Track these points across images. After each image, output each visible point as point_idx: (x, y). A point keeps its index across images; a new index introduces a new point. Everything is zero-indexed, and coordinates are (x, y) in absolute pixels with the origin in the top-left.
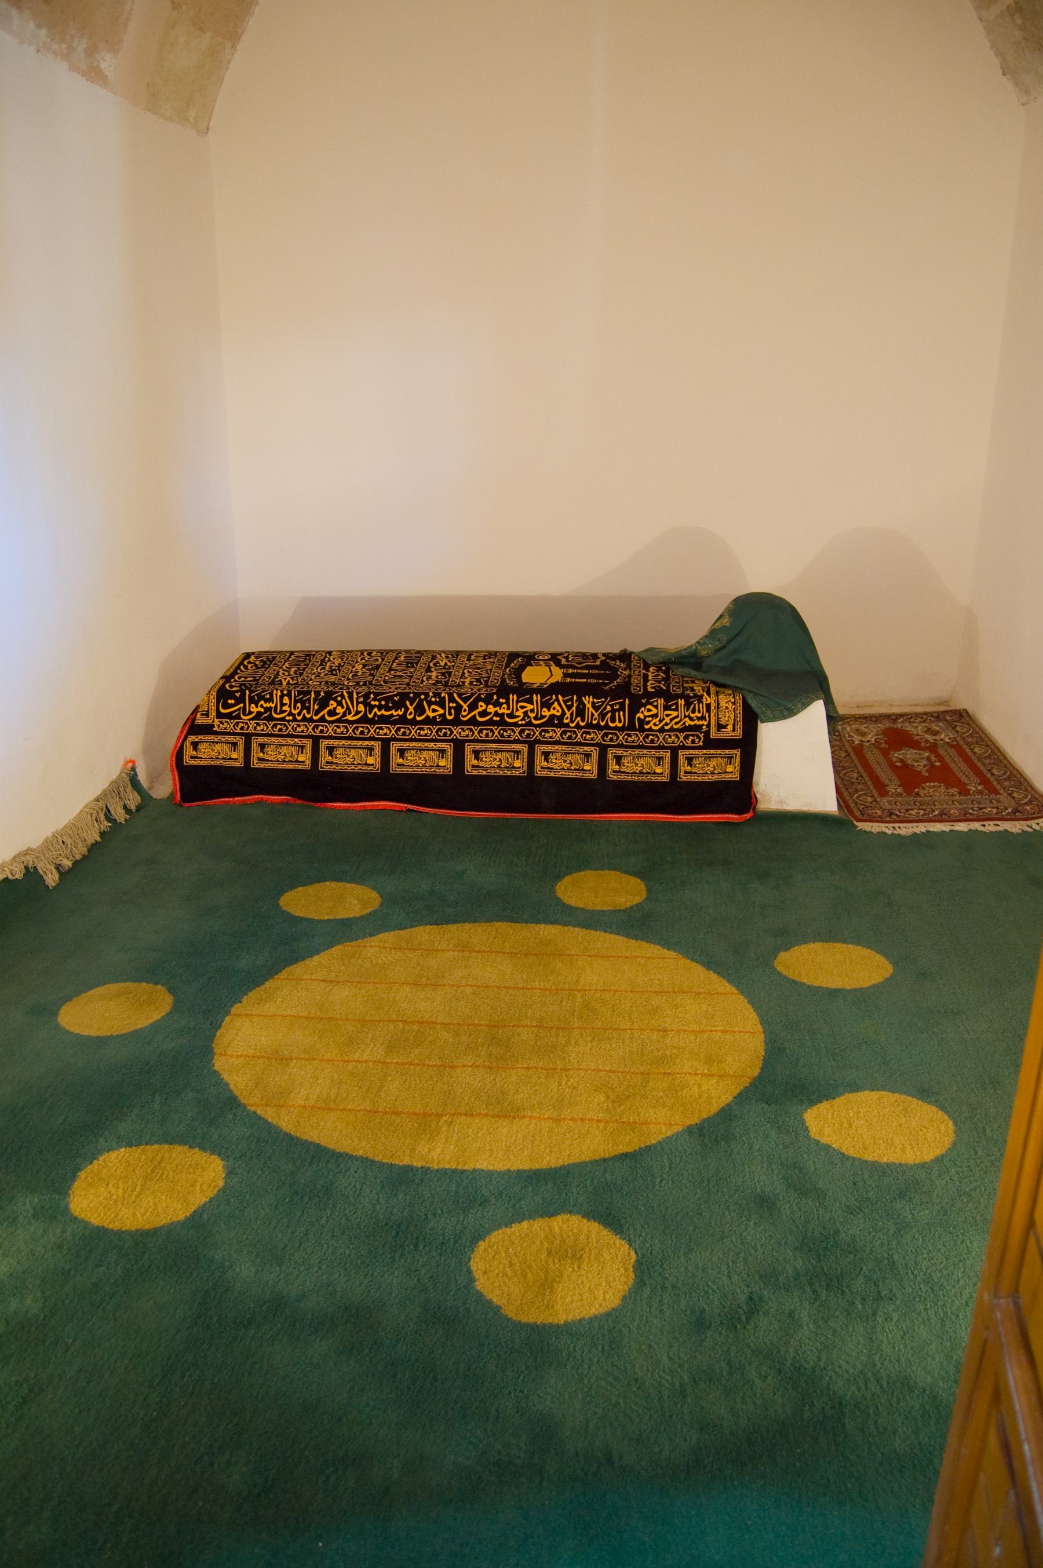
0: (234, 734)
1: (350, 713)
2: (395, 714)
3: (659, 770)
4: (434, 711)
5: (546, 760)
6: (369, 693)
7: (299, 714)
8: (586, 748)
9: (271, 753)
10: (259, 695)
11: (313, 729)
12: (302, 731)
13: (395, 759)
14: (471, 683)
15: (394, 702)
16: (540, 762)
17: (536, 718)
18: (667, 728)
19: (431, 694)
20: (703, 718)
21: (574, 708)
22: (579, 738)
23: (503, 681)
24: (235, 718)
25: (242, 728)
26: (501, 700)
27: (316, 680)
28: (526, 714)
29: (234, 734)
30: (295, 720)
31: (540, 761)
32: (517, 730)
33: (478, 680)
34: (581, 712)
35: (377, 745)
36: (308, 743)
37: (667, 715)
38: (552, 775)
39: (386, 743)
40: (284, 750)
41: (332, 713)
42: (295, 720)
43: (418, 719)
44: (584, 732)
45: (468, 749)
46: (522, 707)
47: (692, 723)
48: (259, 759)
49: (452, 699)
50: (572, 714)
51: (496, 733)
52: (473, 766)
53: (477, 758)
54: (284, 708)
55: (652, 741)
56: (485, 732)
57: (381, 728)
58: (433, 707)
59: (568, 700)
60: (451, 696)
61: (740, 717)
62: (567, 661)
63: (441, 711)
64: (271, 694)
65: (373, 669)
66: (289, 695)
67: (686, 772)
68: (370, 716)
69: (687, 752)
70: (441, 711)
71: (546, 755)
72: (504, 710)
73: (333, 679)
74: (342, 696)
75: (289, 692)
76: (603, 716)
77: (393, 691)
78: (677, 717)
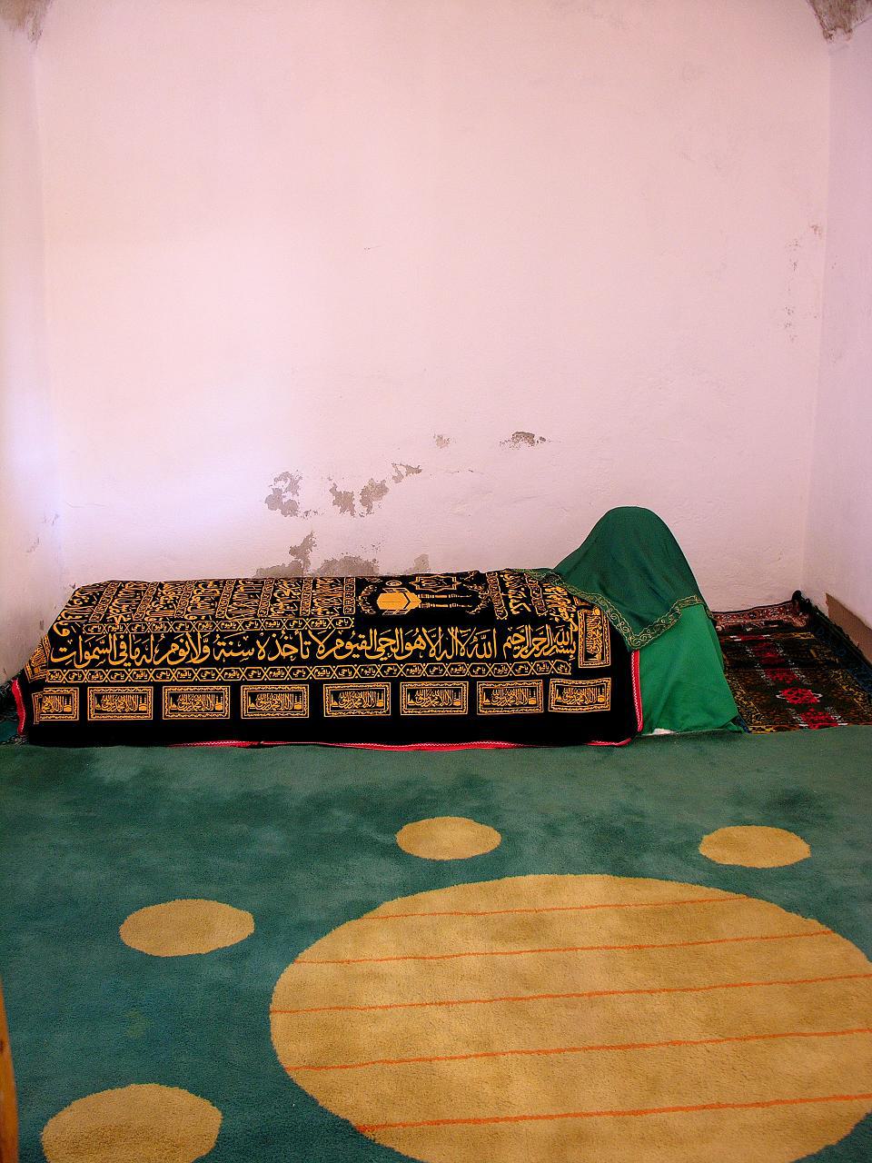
0: (67, 685)
1: (194, 656)
2: (245, 655)
4: (287, 650)
5: (413, 698)
7: (138, 660)
8: (454, 683)
10: (93, 641)
11: (154, 675)
12: (143, 679)
14: (324, 613)
17: (399, 654)
19: (283, 632)
20: (569, 647)
22: (447, 673)
23: (358, 609)
24: (67, 668)
25: (76, 678)
26: (360, 636)
27: (152, 618)
28: (388, 649)
30: (134, 666)
32: (379, 668)
33: (331, 609)
34: (447, 644)
35: (226, 689)
36: (150, 690)
37: (536, 642)
38: (419, 713)
39: (235, 688)
41: (175, 657)
42: (134, 666)
44: (407, 667)
45: (327, 690)
46: (384, 643)
47: (561, 652)
49: (306, 637)
50: (437, 648)
51: (356, 671)
52: (333, 709)
53: (336, 699)
57: (230, 671)
58: (286, 646)
59: (432, 633)
60: (305, 633)
61: (608, 646)
62: (421, 587)
63: (296, 650)
65: (213, 602)
66: (126, 639)
67: (557, 703)
68: (217, 658)
69: (557, 680)
70: (296, 650)
72: (364, 647)
73: (170, 614)
74: (185, 638)
76: (470, 647)
77: (241, 630)
78: (546, 643)
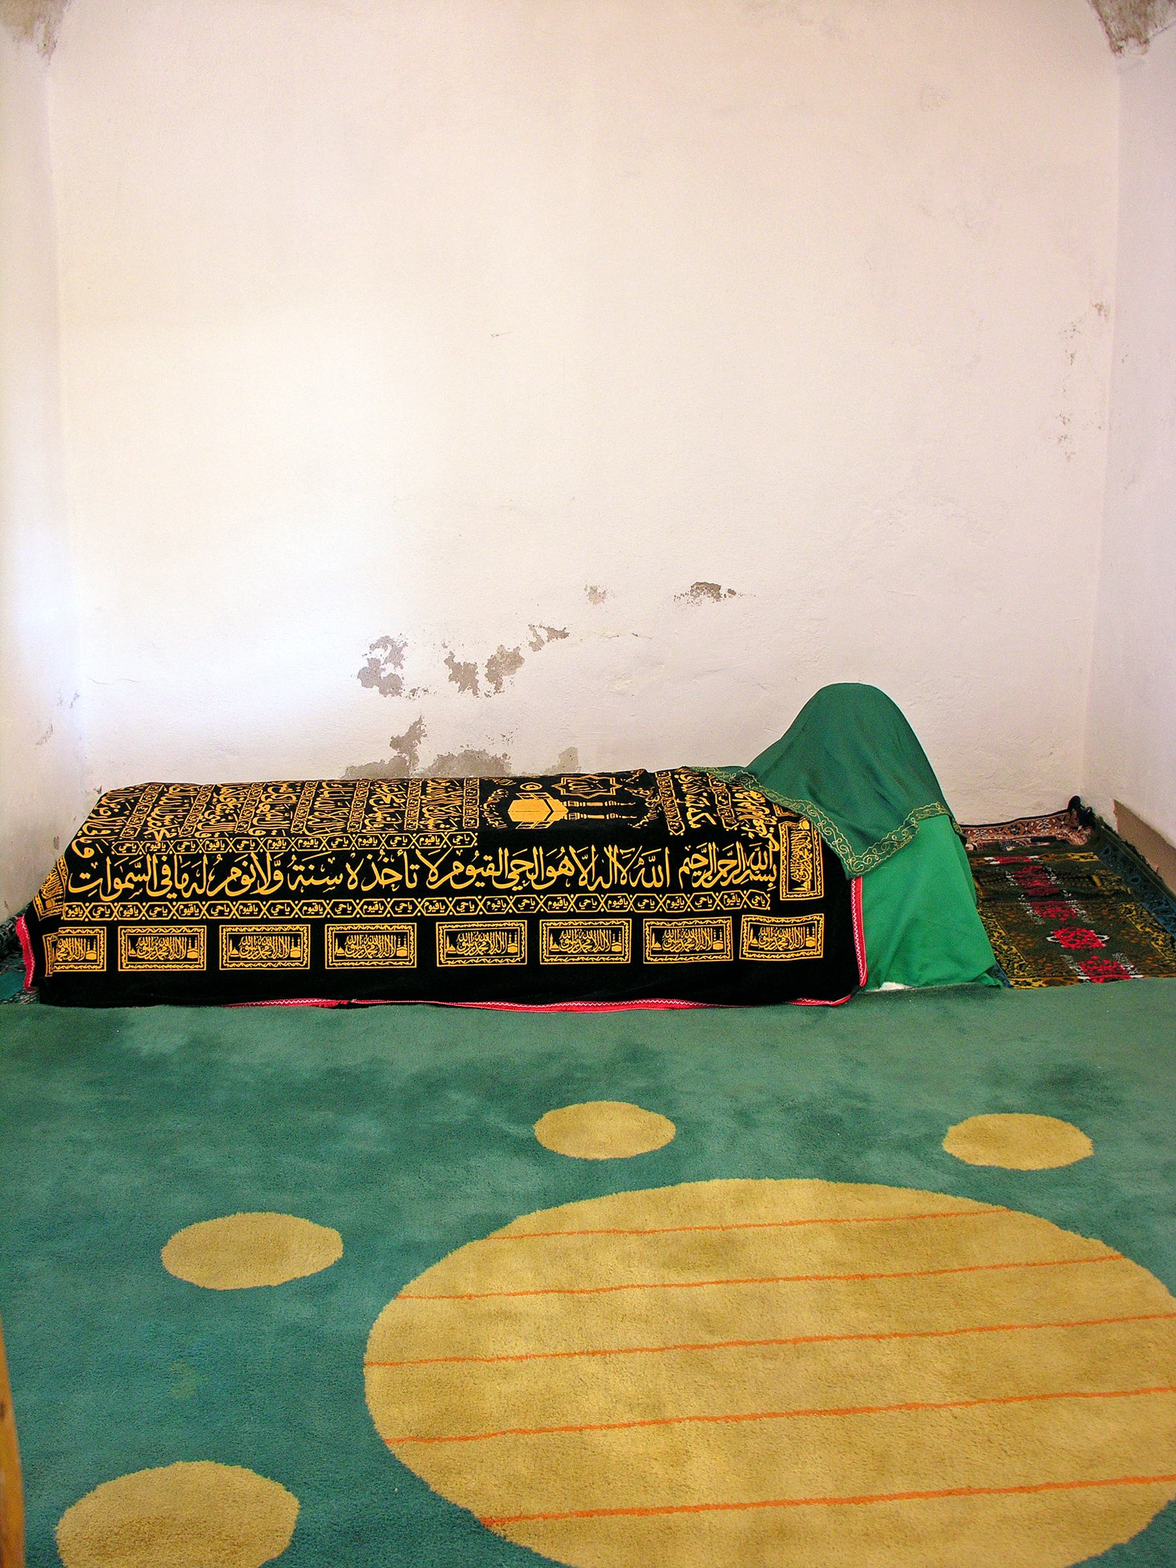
0: (91, 923)
1: (262, 884)
2: (330, 883)
3: (717, 946)
4: (387, 876)
6: (290, 853)
7: (186, 889)
8: (613, 921)
9: (146, 948)
11: (208, 910)
12: (193, 915)
13: (332, 949)
14: (437, 826)
15: (327, 865)
16: (548, 945)
17: (538, 881)
18: (724, 884)
19: (382, 853)
20: (768, 872)
21: (593, 864)
22: (602, 907)
23: (483, 820)
24: (91, 900)
26: (486, 858)
27: (207, 835)
28: (523, 875)
29: (91, 923)
30: (180, 898)
31: (546, 943)
32: (511, 900)
33: (446, 822)
34: (603, 869)
35: (304, 930)
36: (202, 931)
37: (723, 866)
38: (566, 962)
39: (318, 927)
40: (167, 943)
41: (236, 885)
42: (180, 898)
43: (364, 889)
44: (609, 898)
45: (441, 929)
46: (517, 866)
47: (756, 878)
48: (130, 959)
49: (413, 859)
50: (590, 873)
51: (481, 905)
53: (453, 942)
54: (163, 882)
55: (705, 905)
56: (464, 904)
57: (310, 905)
58: (386, 870)
59: (583, 854)
60: (411, 853)
61: (820, 870)
62: (568, 791)
63: (398, 877)
64: (144, 861)
65: (286, 810)
66: (170, 862)
67: (751, 948)
69: (753, 917)
70: (398, 877)
71: (556, 934)
72: (490, 872)
73: (230, 827)
74: (250, 860)
75: (170, 857)
76: (633, 873)
77: (325, 850)
78: (736, 867)
